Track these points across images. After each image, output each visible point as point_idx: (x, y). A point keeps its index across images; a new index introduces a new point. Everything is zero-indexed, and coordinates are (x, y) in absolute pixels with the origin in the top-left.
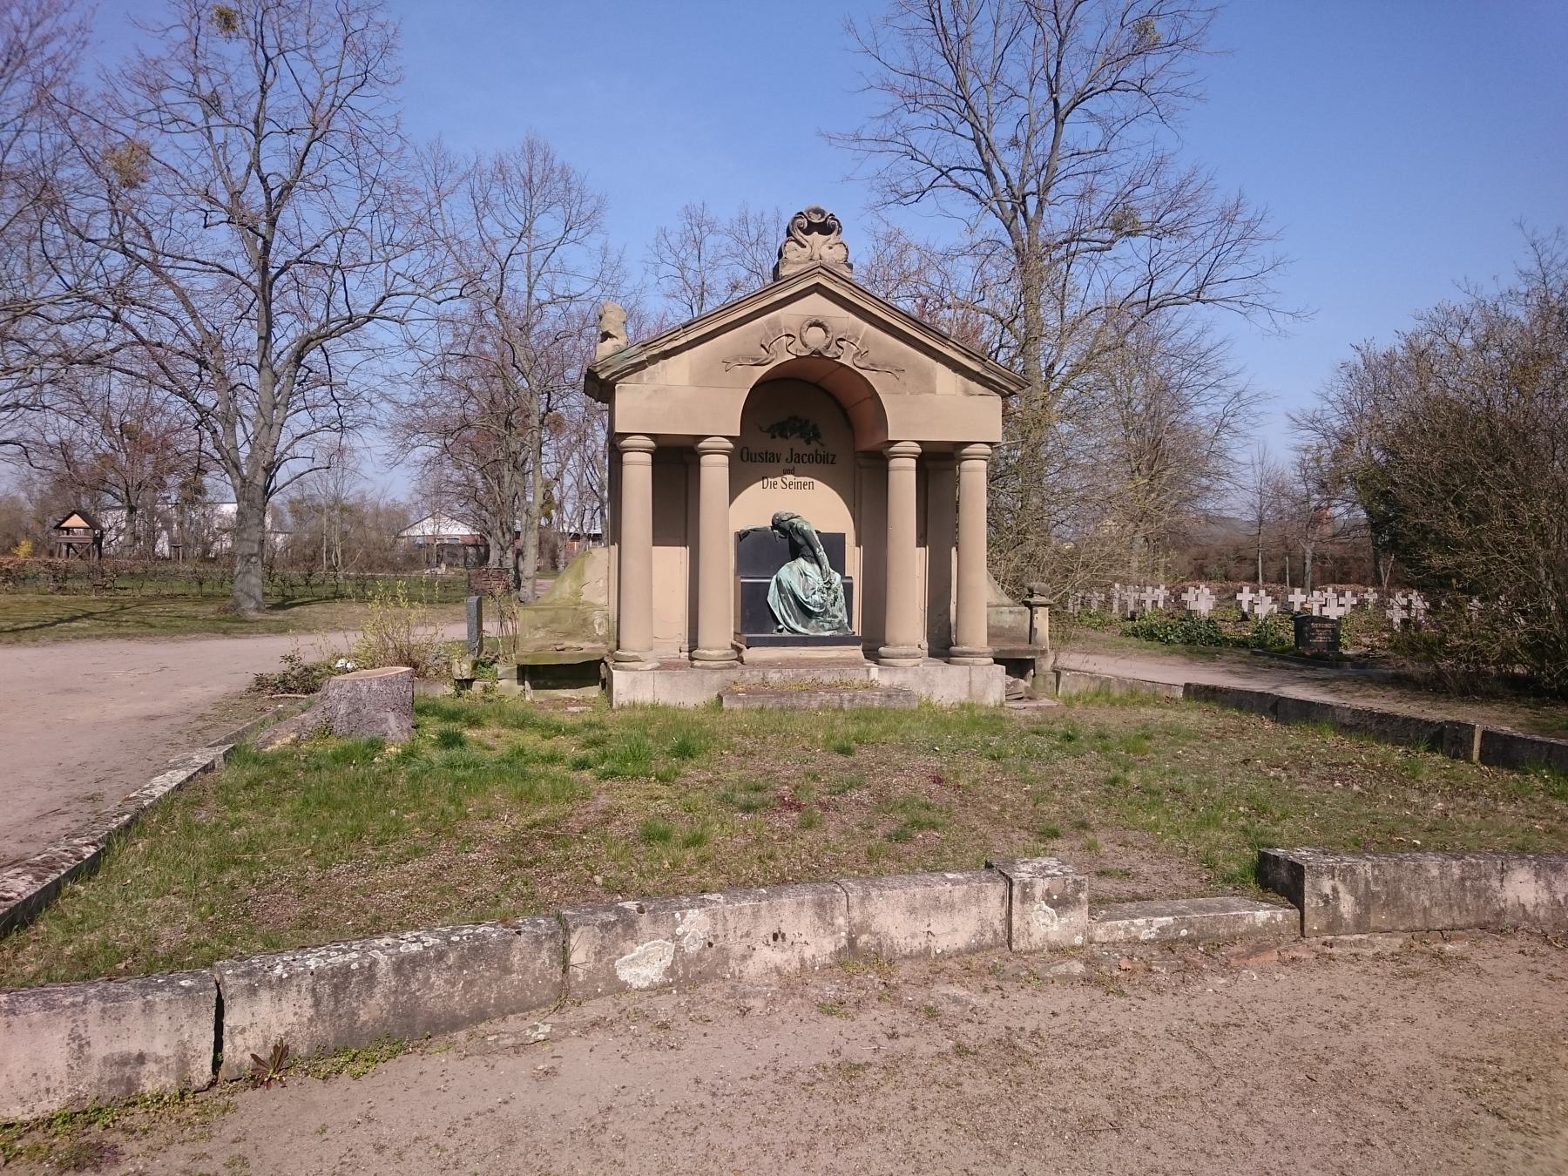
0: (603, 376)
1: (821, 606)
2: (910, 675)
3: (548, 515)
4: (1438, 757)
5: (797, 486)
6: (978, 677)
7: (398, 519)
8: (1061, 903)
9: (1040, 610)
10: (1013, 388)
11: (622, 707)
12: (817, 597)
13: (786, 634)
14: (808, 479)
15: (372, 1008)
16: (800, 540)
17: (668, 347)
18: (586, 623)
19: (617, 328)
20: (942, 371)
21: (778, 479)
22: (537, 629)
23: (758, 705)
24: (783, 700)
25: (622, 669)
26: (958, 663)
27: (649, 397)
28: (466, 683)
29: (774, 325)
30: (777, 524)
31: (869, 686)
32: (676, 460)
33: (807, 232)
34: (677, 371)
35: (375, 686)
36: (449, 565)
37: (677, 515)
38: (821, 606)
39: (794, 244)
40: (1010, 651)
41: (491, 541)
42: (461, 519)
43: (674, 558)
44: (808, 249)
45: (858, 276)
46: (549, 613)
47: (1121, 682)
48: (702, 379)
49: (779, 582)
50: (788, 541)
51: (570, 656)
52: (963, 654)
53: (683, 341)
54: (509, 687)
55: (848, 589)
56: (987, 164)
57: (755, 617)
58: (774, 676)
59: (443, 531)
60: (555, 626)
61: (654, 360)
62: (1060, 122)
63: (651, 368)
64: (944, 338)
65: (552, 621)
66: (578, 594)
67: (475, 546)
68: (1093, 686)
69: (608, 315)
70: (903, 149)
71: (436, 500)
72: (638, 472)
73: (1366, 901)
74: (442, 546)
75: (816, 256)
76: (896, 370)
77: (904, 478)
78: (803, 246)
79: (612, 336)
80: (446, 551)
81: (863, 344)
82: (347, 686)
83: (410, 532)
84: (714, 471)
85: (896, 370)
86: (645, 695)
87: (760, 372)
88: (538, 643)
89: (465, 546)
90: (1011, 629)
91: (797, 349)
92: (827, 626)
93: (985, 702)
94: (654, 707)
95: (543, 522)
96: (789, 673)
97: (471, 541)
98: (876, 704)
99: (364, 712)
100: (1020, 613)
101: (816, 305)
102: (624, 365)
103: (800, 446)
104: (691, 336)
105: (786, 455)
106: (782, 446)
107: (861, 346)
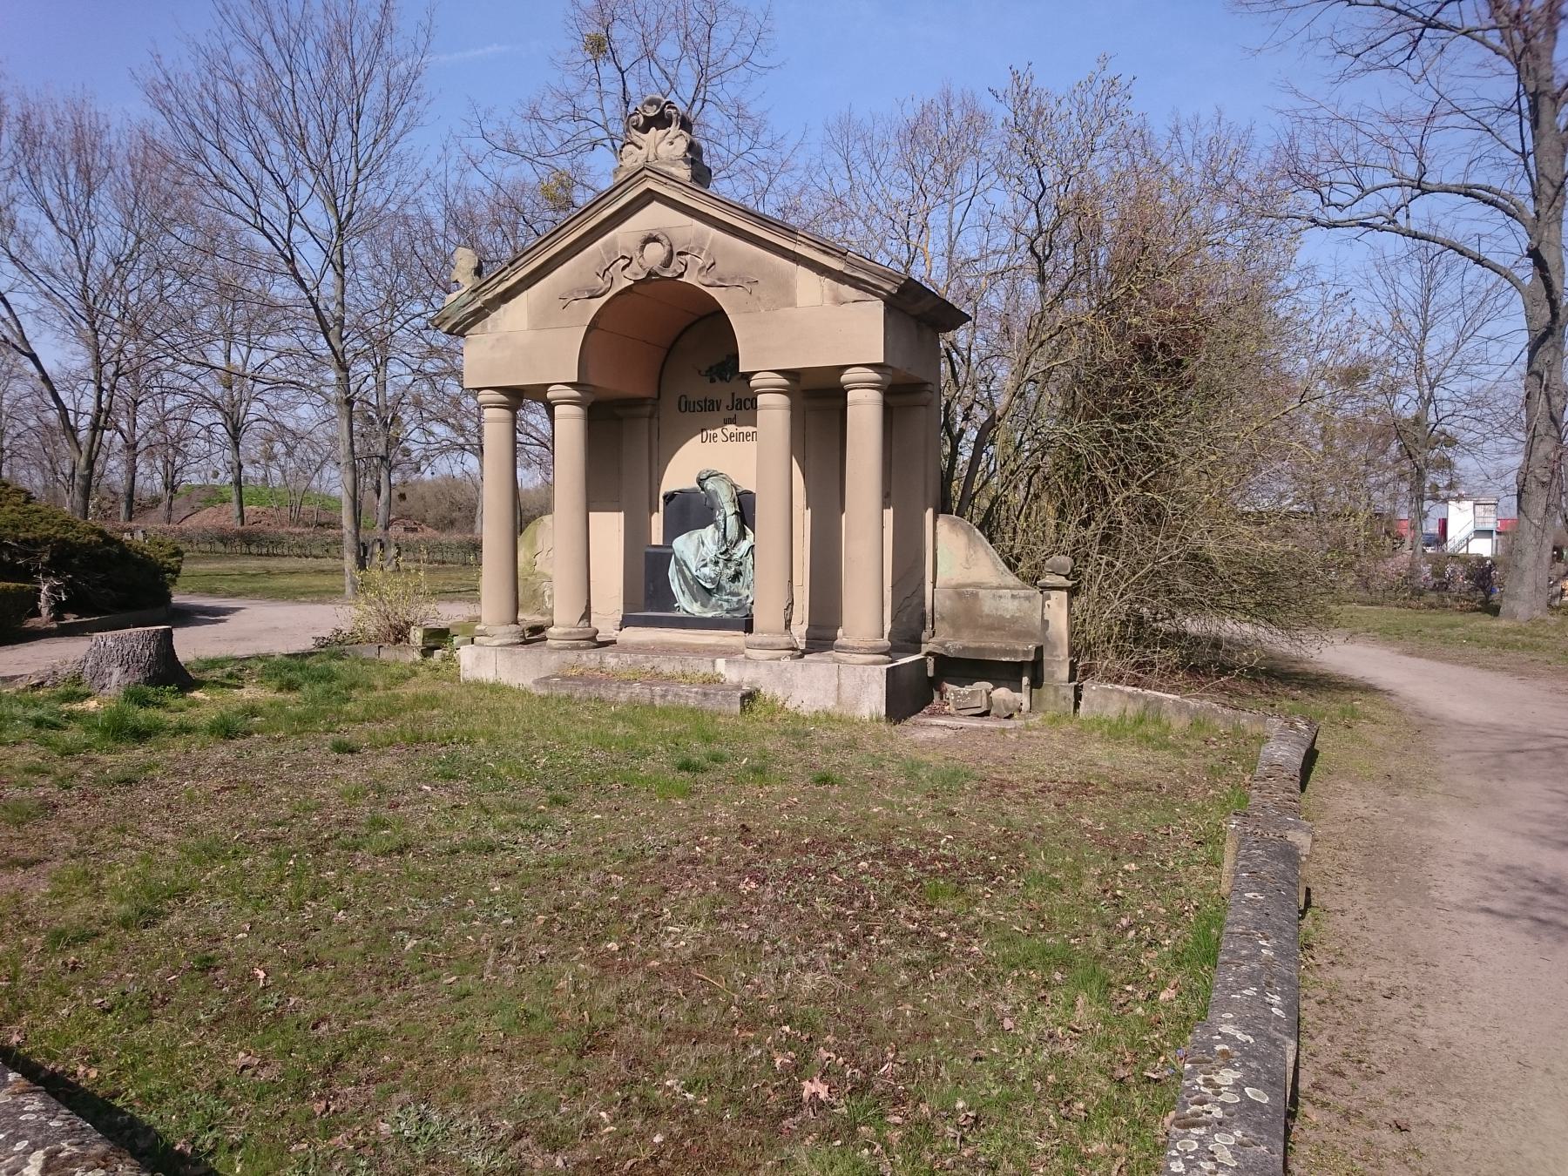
2: (763, 671)
6: (849, 681)
9: (1054, 594)
20: (802, 271)
21: (718, 431)
24: (591, 689)
27: (492, 347)
40: (978, 649)
43: (609, 528)
44: (644, 151)
48: (541, 321)
52: (843, 648)
53: (514, 280)
64: (791, 232)
81: (709, 255)
86: (487, 674)
90: (1014, 620)
91: (636, 272)
93: (858, 714)
100: (1027, 598)
105: (727, 401)
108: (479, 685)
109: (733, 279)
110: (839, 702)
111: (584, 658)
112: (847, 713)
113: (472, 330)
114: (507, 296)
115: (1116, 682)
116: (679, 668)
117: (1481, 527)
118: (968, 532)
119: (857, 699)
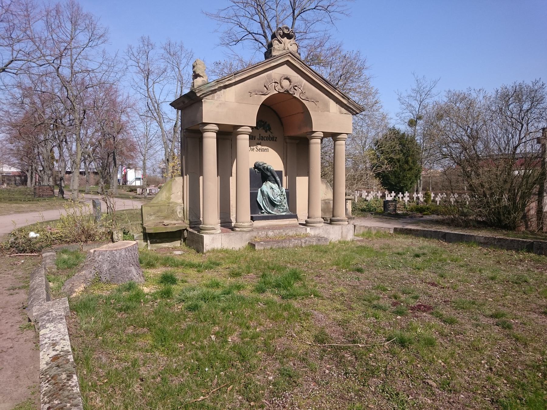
0: (198, 95)
1: (280, 202)
2: (321, 230)
4: (532, 255)
5: (262, 150)
10: (358, 112)
11: (208, 251)
12: (278, 198)
13: (266, 214)
14: (266, 148)
16: (269, 174)
17: (227, 83)
18: (173, 212)
19: (203, 72)
20: (332, 103)
21: (255, 147)
22: (151, 215)
23: (269, 247)
24: (279, 244)
25: (207, 233)
26: (337, 225)
27: (218, 107)
29: (269, 77)
31: (307, 236)
32: (227, 135)
33: (282, 37)
34: (230, 95)
35: (123, 253)
36: (8, 184)
38: (280, 202)
39: (277, 42)
42: (13, 165)
44: (283, 45)
45: (302, 58)
46: (157, 208)
47: (375, 228)
48: (241, 99)
49: (262, 192)
51: (172, 228)
52: (338, 220)
53: (233, 81)
56: (264, 32)
58: (271, 234)
60: (159, 214)
61: (220, 89)
62: (294, 19)
63: (218, 93)
64: (335, 89)
65: (158, 211)
66: (169, 198)
68: (367, 230)
69: (198, 66)
70: (236, 22)
72: (210, 141)
75: (286, 48)
76: (315, 101)
78: (281, 43)
79: (200, 76)
81: (303, 89)
82: (107, 254)
84: (243, 141)
85: (315, 101)
86: (218, 245)
87: (264, 98)
89: (15, 176)
92: (281, 210)
93: (347, 240)
94: (222, 251)
96: (277, 232)
97: (17, 174)
98: (314, 244)
99: (118, 267)
101: (285, 70)
102: (208, 90)
104: (237, 79)
107: (305, 90)
108: (213, 250)
109: (311, 99)
110: (342, 237)
111: (260, 234)
112: (344, 239)
113: (207, 97)
114: (226, 87)
115: (24, 252)
116: (295, 233)
117: (137, 177)
118: (326, 184)
119: (347, 235)
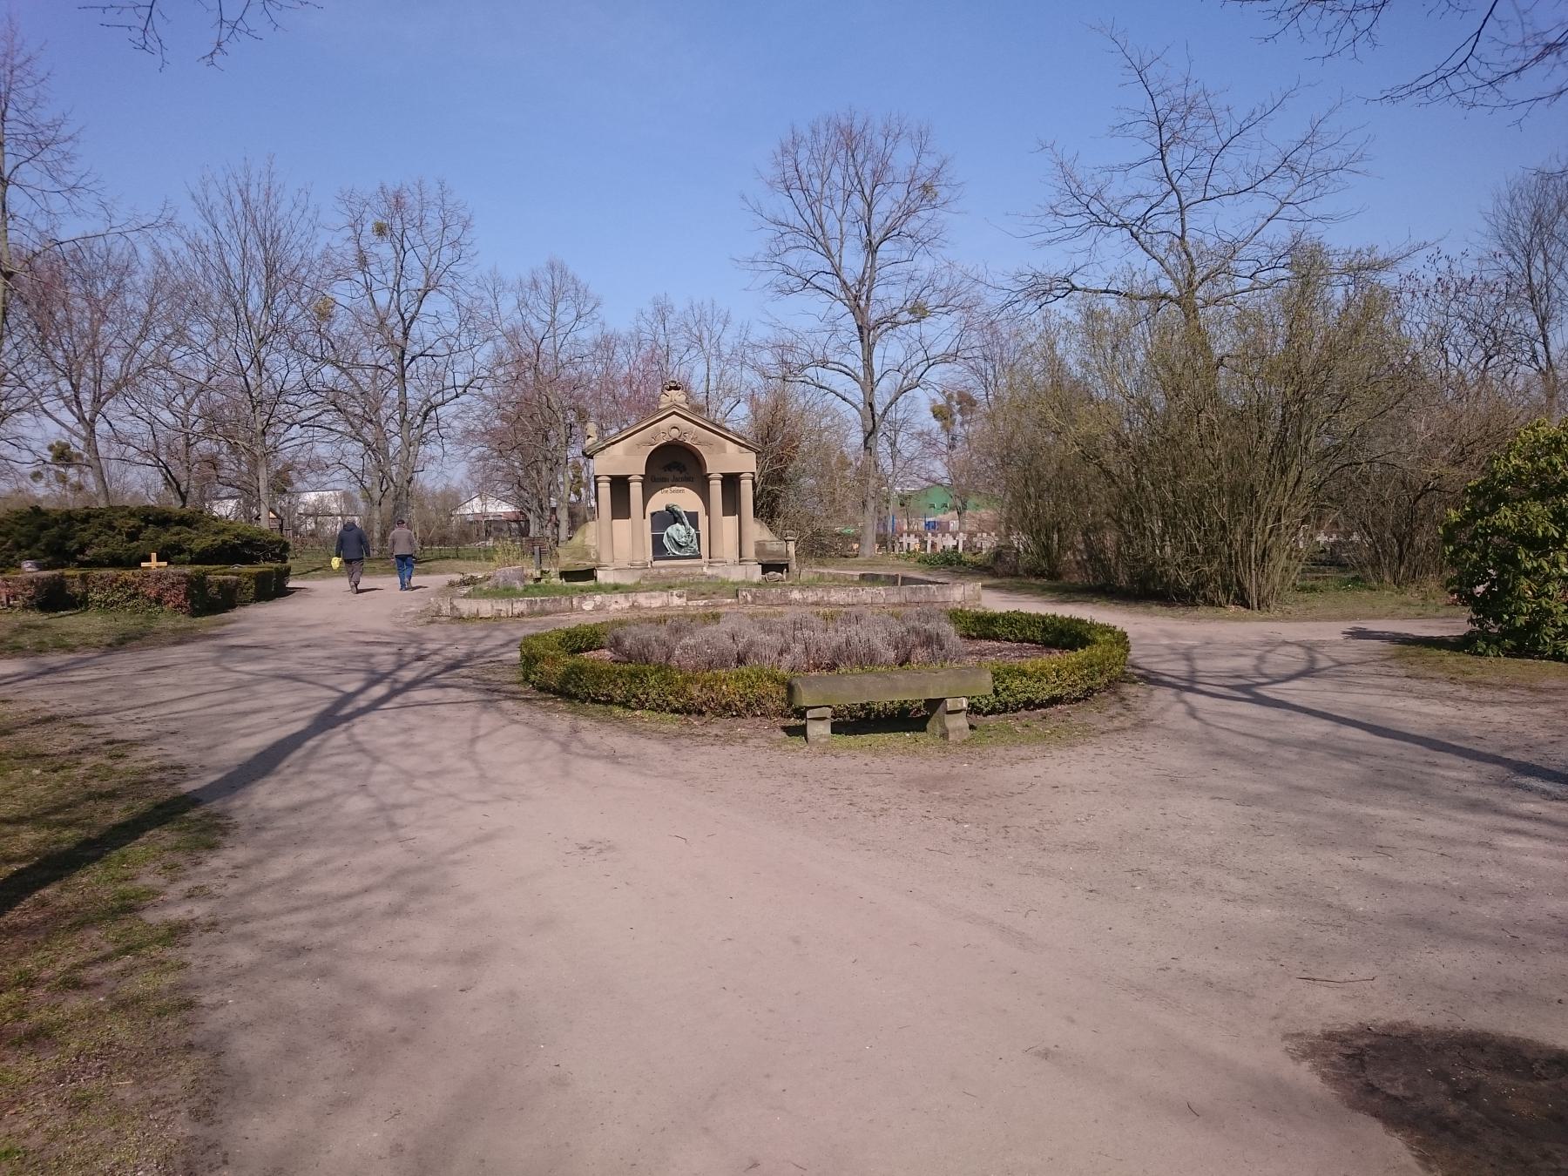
3: (577, 493)
7: (452, 500)
8: (680, 597)
15: (536, 608)
18: (588, 554)
28: (538, 580)
29: (657, 429)
30: (668, 509)
32: (620, 485)
36: (496, 539)
37: (621, 508)
41: (531, 517)
42: (505, 499)
48: (629, 452)
50: (672, 516)
54: (557, 581)
55: (698, 536)
57: (659, 549)
59: (490, 510)
67: (517, 521)
71: (485, 489)
73: (754, 597)
74: (489, 523)
77: (716, 488)
80: (492, 527)
83: (461, 511)
84: (636, 490)
88: (567, 561)
95: (573, 498)
101: (674, 420)
103: (677, 474)
106: (670, 475)
107: (693, 435)
